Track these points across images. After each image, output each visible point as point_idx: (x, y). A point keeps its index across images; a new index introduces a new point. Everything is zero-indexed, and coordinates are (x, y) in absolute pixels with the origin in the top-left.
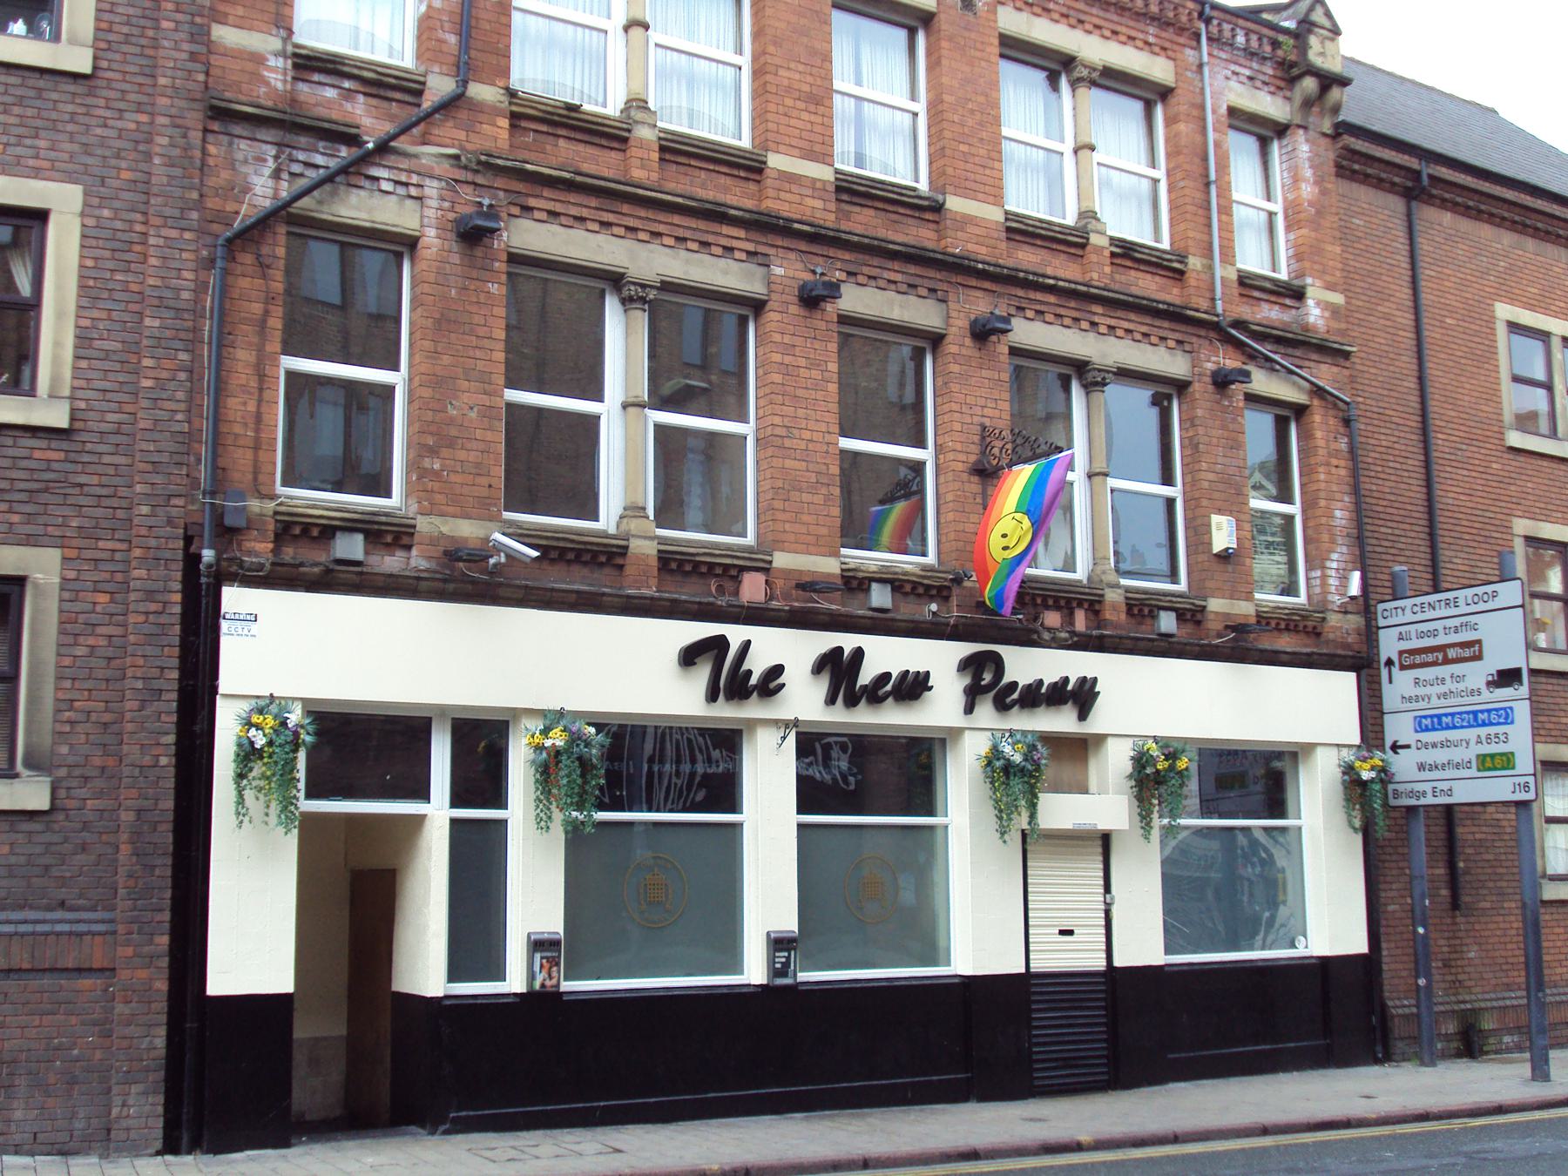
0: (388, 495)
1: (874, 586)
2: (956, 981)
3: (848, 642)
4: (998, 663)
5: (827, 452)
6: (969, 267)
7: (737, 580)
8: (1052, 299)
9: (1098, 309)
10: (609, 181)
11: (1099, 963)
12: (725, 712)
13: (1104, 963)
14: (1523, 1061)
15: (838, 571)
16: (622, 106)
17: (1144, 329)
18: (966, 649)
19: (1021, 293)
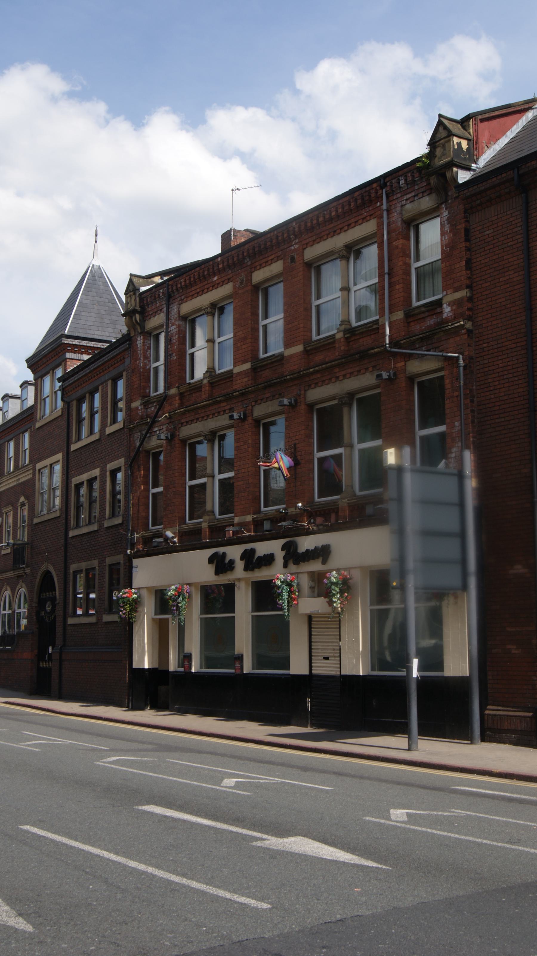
0: (319, 497)
1: (265, 522)
2: (289, 676)
3: (249, 546)
4: (253, 551)
5: (248, 475)
6: (285, 380)
7: (262, 524)
8: (319, 375)
9: (337, 370)
10: (190, 406)
11: (306, 672)
12: (225, 579)
13: (339, 673)
14: (406, 737)
15: (252, 520)
16: (205, 372)
17: (357, 369)
18: (283, 541)
19: (307, 379)
